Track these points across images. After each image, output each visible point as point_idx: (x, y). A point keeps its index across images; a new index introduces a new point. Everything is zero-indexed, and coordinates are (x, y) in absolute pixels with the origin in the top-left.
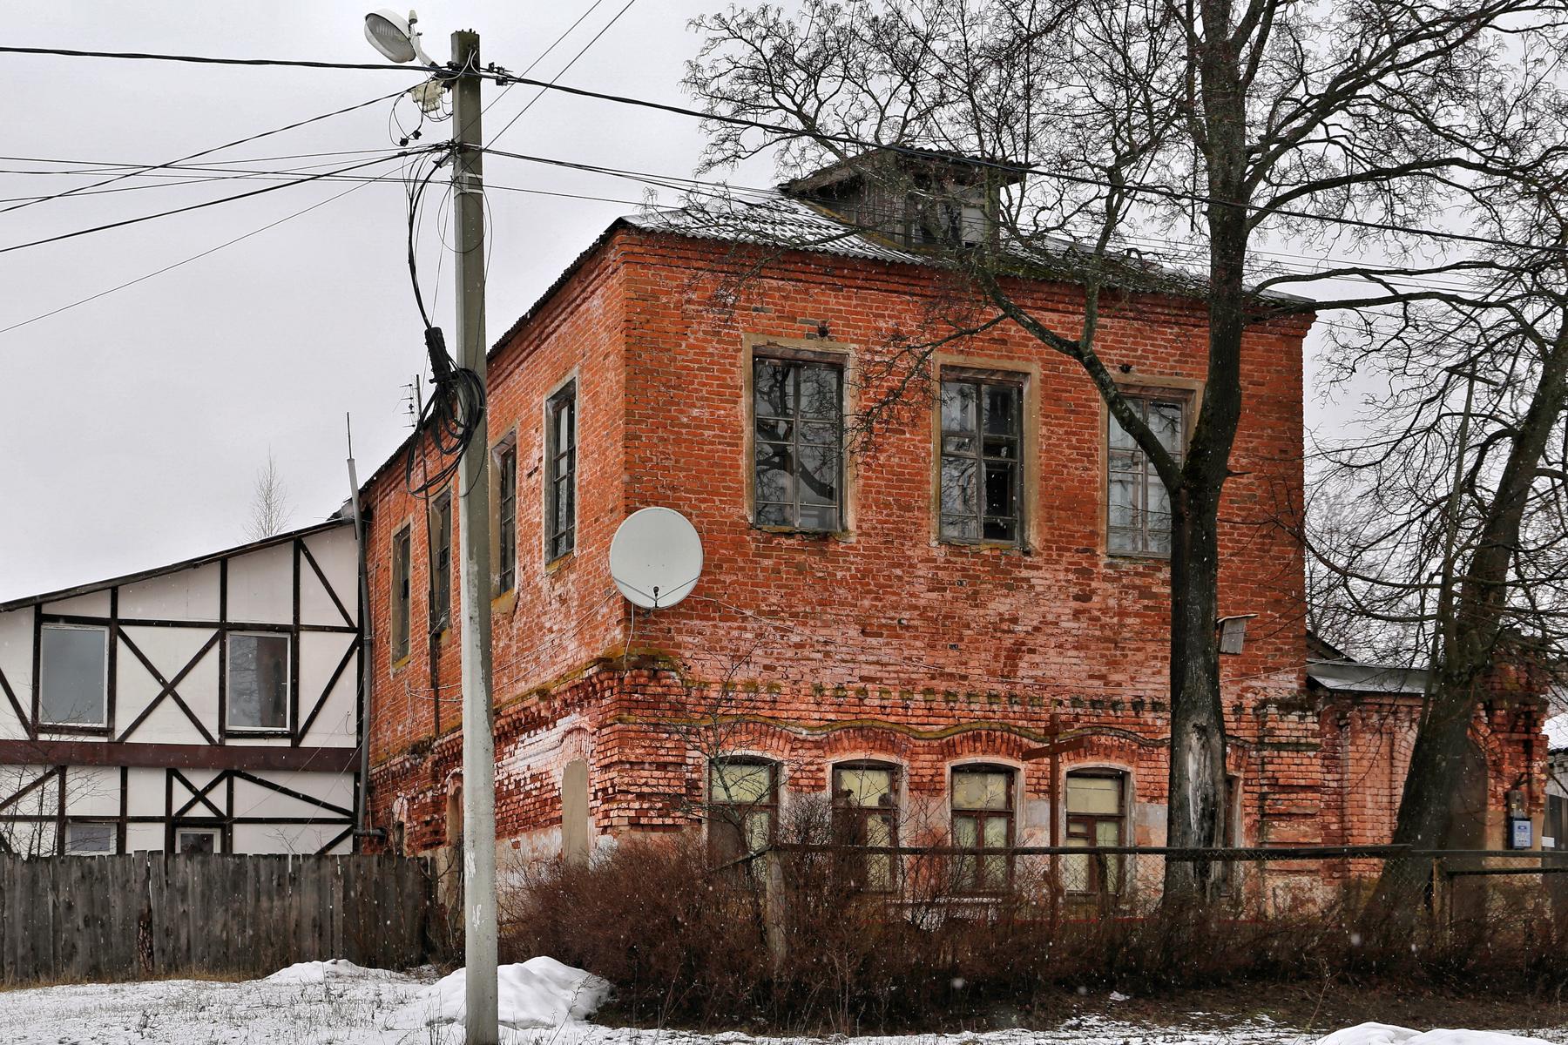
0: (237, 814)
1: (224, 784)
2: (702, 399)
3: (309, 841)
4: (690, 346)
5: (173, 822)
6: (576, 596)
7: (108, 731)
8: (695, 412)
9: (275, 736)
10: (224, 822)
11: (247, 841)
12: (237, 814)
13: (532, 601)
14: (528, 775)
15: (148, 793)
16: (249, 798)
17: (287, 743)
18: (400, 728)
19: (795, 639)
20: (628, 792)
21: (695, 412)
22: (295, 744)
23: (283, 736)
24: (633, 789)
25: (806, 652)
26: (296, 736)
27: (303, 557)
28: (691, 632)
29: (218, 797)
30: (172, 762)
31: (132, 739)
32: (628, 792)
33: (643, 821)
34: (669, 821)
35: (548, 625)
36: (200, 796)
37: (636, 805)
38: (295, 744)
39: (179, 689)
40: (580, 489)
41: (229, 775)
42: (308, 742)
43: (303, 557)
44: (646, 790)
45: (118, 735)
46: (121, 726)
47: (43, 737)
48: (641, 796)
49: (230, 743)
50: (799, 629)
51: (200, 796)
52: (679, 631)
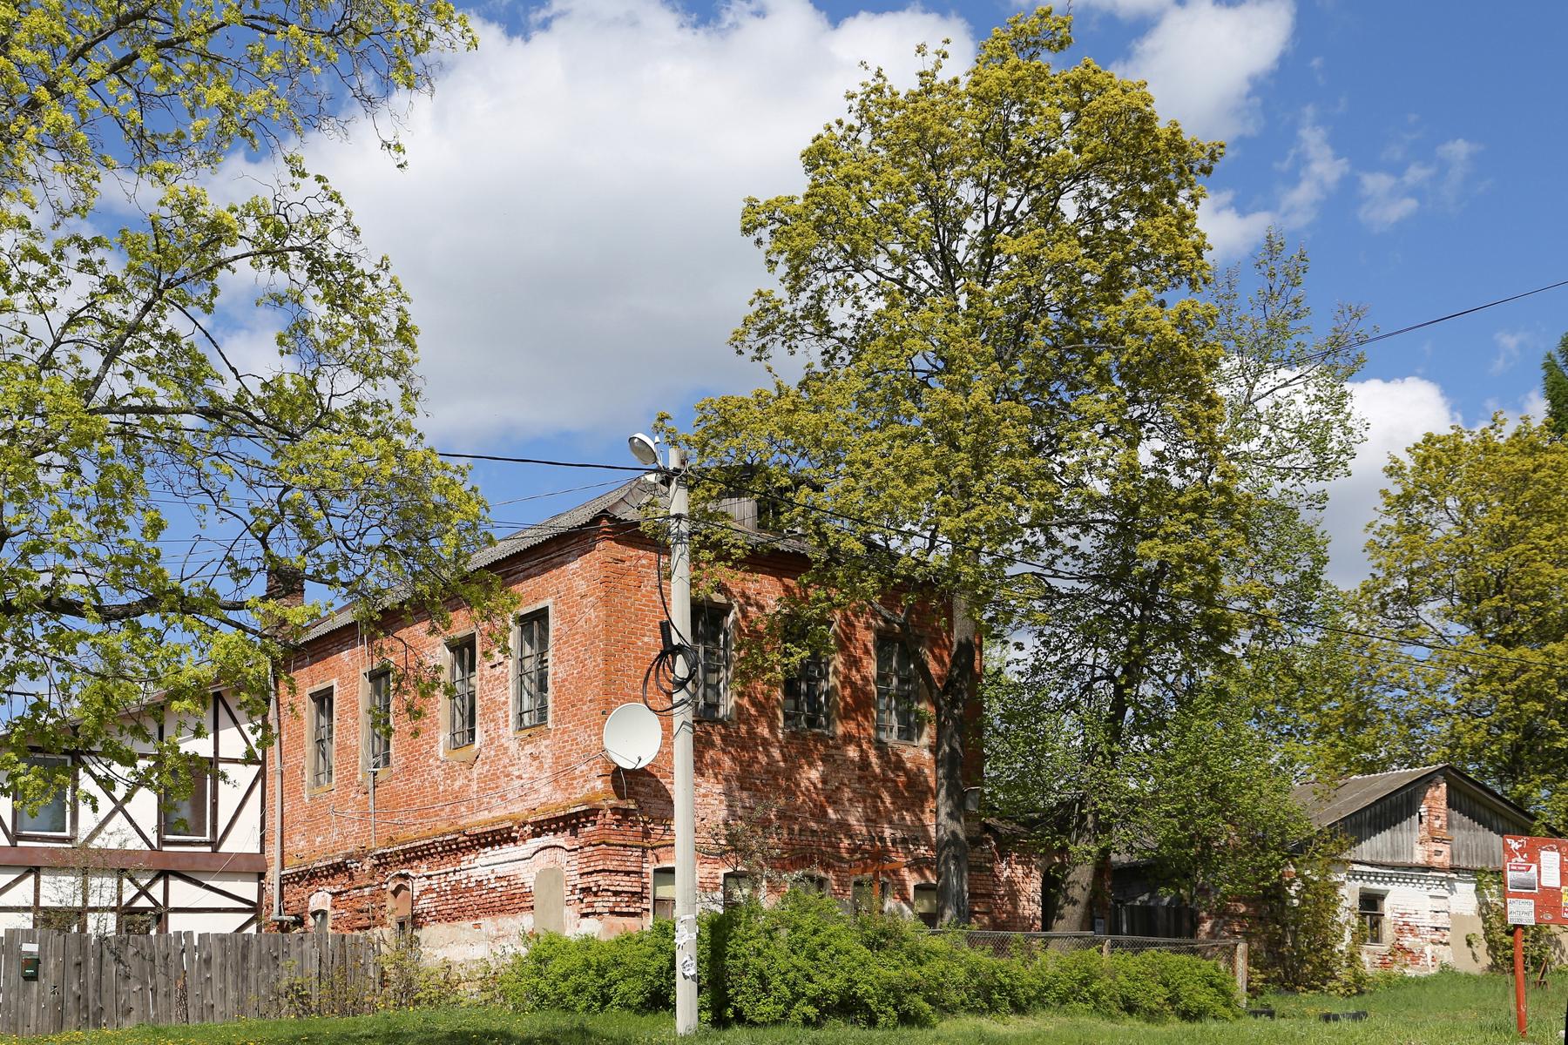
0: (171, 905)
1: (161, 883)
2: (650, 630)
3: (228, 924)
4: (643, 596)
5: (126, 912)
6: (550, 756)
7: (70, 840)
8: (646, 639)
9: (200, 844)
10: (160, 914)
11: (176, 923)
12: (171, 905)
13: (496, 755)
14: (493, 876)
15: (104, 890)
16: (181, 893)
17: (208, 849)
18: (319, 839)
19: (702, 791)
20: (608, 890)
21: (646, 639)
22: (215, 851)
23: (206, 844)
24: (612, 888)
25: (709, 800)
26: (215, 844)
27: (221, 706)
28: (643, 785)
29: (157, 891)
30: (120, 866)
31: (97, 843)
32: (608, 890)
33: (617, 909)
34: (632, 910)
35: (517, 773)
36: (143, 892)
37: (613, 899)
38: (215, 851)
39: (127, 807)
40: (554, 683)
41: (164, 874)
42: (224, 849)
43: (221, 706)
44: (619, 889)
45: (80, 841)
46: (83, 834)
47: (20, 844)
48: (616, 893)
49: (165, 849)
50: (704, 785)
51: (143, 892)
52: (637, 784)
